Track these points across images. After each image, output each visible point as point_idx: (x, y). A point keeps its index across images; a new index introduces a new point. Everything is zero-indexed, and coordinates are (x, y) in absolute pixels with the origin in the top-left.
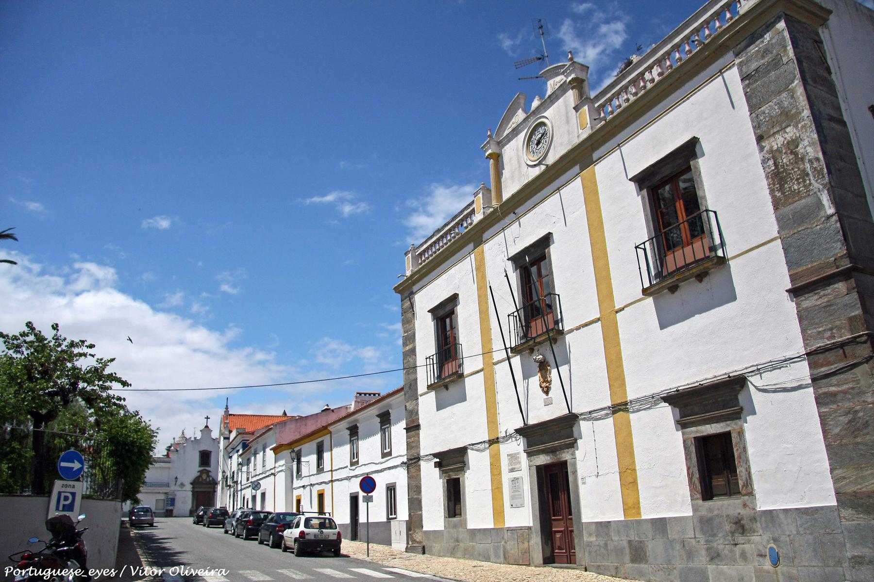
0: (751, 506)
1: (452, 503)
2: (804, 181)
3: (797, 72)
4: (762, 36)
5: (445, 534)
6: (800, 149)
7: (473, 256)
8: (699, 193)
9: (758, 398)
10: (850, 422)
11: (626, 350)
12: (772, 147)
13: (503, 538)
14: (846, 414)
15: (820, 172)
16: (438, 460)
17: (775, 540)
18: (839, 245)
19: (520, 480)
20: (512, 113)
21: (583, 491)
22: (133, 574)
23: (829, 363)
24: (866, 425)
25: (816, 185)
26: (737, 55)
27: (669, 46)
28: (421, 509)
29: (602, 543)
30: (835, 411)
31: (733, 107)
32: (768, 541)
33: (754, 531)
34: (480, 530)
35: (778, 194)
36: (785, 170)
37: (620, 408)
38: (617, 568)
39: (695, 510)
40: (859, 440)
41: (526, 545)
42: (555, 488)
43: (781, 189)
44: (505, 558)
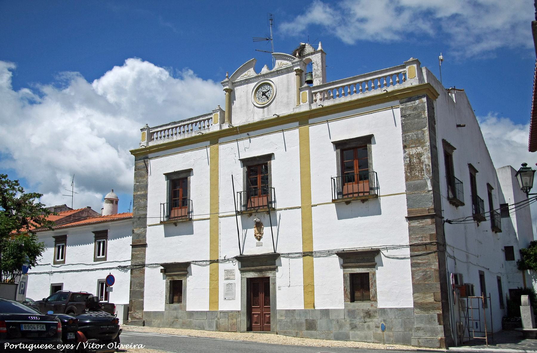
1: (171, 295)
2: (421, 173)
3: (427, 124)
4: (415, 100)
5: (165, 313)
6: (422, 158)
7: (209, 149)
8: (369, 161)
9: (384, 259)
11: (315, 226)
12: (410, 153)
13: (216, 317)
14: (423, 272)
15: (429, 171)
16: (163, 268)
17: (384, 321)
18: (431, 204)
19: (233, 285)
20: (246, 68)
21: (278, 293)
22: (85, 348)
23: (419, 251)
24: (430, 277)
25: (426, 176)
26: (401, 103)
27: (363, 80)
28: (143, 297)
29: (289, 320)
30: (418, 270)
32: (381, 321)
33: (375, 317)
34: (197, 312)
35: (409, 174)
36: (414, 165)
37: (308, 254)
38: (297, 333)
39: (346, 306)
40: (426, 282)
41: (235, 320)
42: (259, 292)
43: (410, 172)
44: (217, 328)
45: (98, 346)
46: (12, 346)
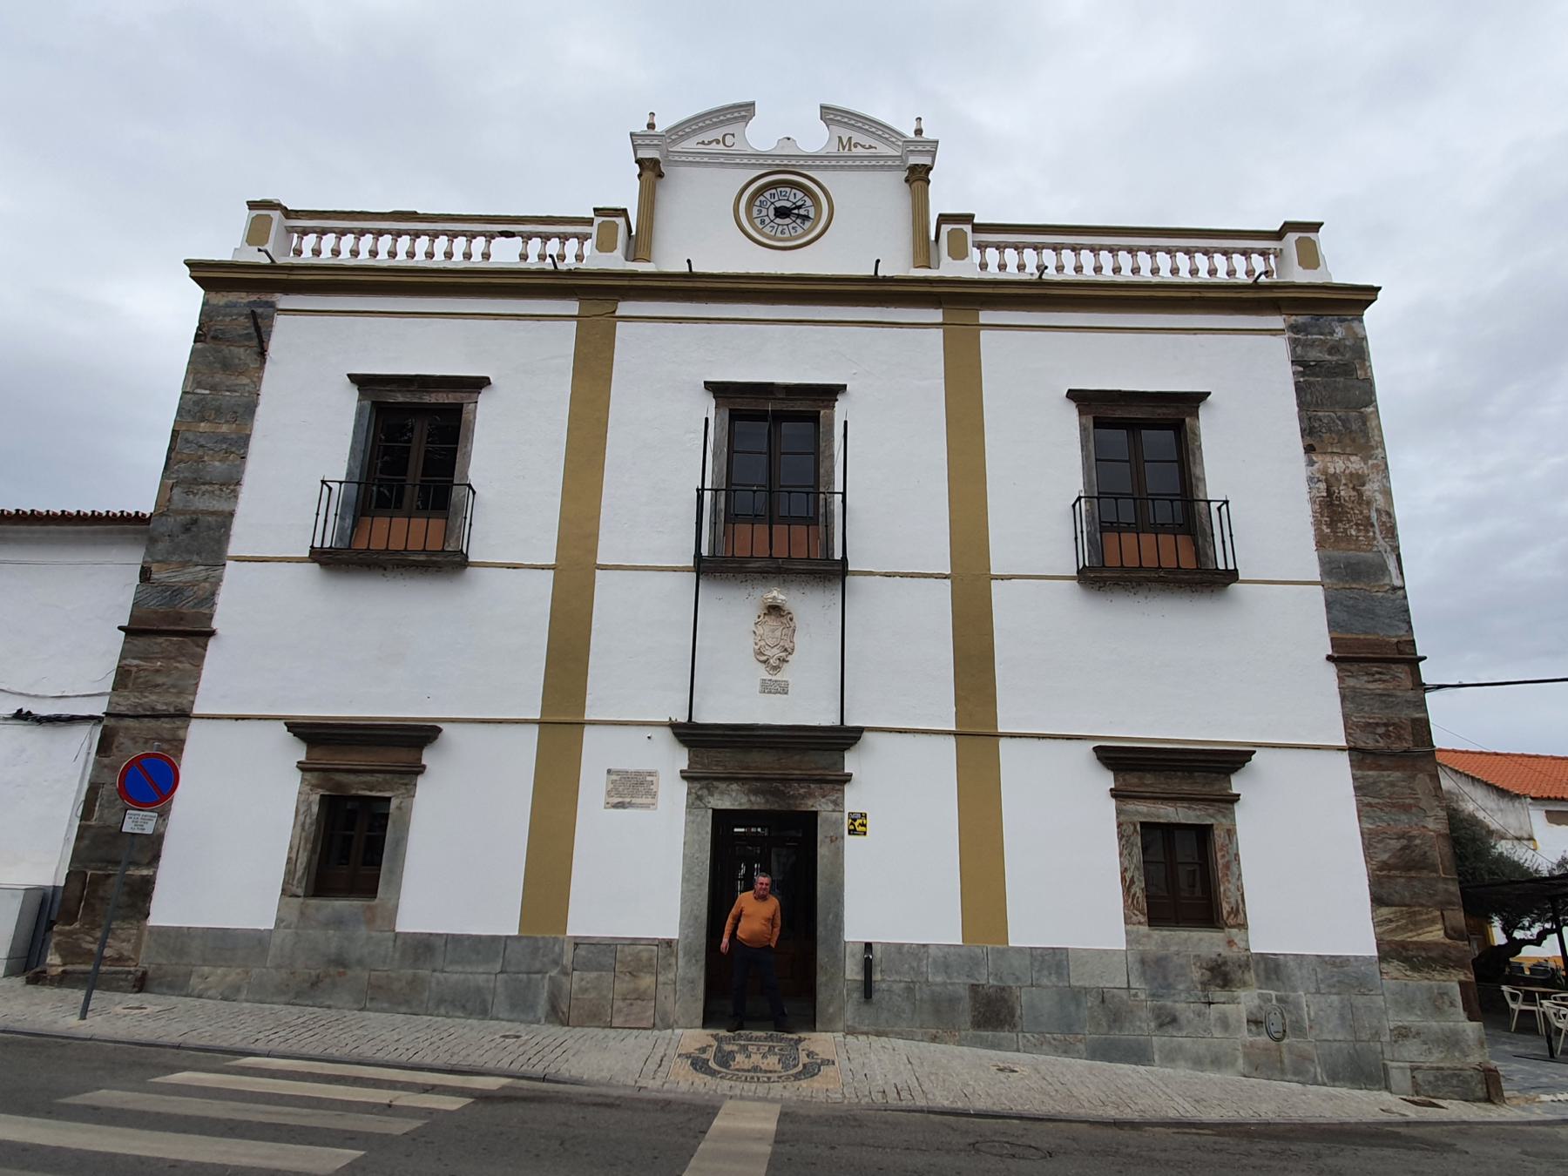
0: (1242, 944)
10: (1404, 848)
31: (21, 716)
39: (1131, 939)
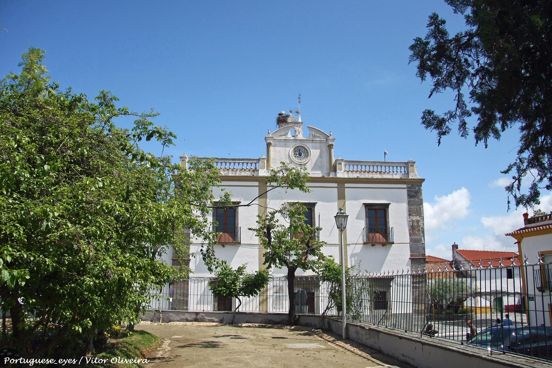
22: (87, 362)
45: (100, 361)
46: (12, 361)
